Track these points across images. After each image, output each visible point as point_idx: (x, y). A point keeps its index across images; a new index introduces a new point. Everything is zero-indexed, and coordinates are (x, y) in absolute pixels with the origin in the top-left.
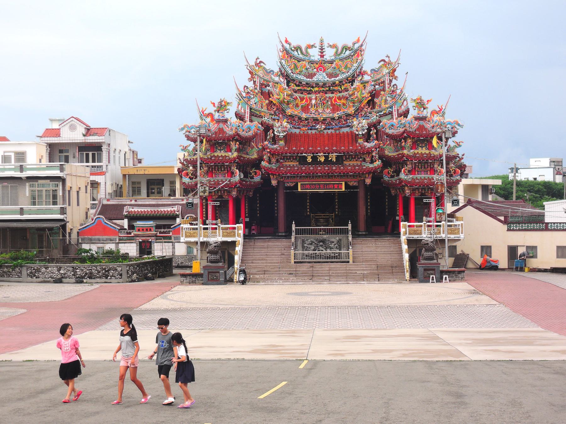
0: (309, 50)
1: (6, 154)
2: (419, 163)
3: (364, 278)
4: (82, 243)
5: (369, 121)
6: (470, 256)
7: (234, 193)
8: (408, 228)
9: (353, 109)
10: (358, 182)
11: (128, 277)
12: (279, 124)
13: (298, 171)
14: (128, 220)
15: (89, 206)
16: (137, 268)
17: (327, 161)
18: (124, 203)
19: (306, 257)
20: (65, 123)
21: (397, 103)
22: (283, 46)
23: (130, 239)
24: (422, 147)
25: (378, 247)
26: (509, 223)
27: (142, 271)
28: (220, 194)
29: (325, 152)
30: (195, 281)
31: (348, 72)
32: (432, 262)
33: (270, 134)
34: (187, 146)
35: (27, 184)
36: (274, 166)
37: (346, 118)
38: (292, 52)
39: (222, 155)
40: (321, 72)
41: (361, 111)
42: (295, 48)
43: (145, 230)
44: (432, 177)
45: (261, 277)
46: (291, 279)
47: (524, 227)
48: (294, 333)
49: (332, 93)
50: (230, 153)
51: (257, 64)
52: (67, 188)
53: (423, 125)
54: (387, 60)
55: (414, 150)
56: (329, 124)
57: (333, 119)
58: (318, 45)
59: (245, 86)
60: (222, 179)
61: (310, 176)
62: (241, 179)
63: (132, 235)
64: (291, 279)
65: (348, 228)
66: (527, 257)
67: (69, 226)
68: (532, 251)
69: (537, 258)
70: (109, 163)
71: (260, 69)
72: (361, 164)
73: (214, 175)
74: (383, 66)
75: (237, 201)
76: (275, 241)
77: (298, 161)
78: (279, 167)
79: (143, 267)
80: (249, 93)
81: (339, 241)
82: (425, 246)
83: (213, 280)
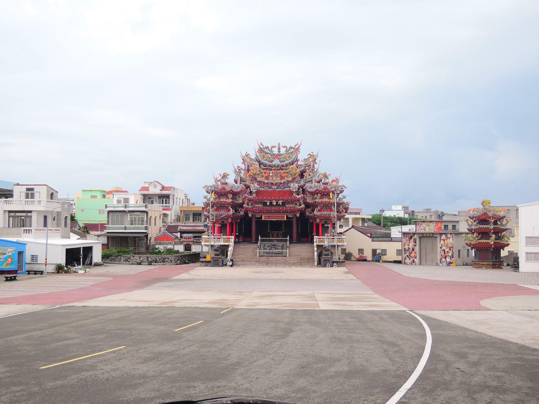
1: (119, 199)
3: (293, 264)
5: (300, 185)
6: (353, 254)
7: (229, 220)
8: (318, 239)
9: (291, 178)
12: (253, 185)
13: (262, 210)
15: (161, 226)
18: (179, 225)
20: (151, 184)
22: (259, 146)
23: (181, 243)
24: (326, 198)
26: (373, 238)
27: (183, 259)
29: (276, 200)
35: (129, 215)
36: (250, 207)
38: (264, 150)
41: (295, 179)
43: (188, 238)
48: (242, 292)
49: (282, 170)
50: (228, 200)
51: (246, 156)
52: (149, 217)
54: (312, 154)
56: (279, 186)
58: (277, 146)
59: (238, 166)
60: (223, 213)
62: (233, 213)
63: (181, 241)
65: (287, 239)
66: (381, 255)
67: (149, 236)
68: (384, 252)
70: (173, 204)
78: (253, 207)
79: (183, 257)
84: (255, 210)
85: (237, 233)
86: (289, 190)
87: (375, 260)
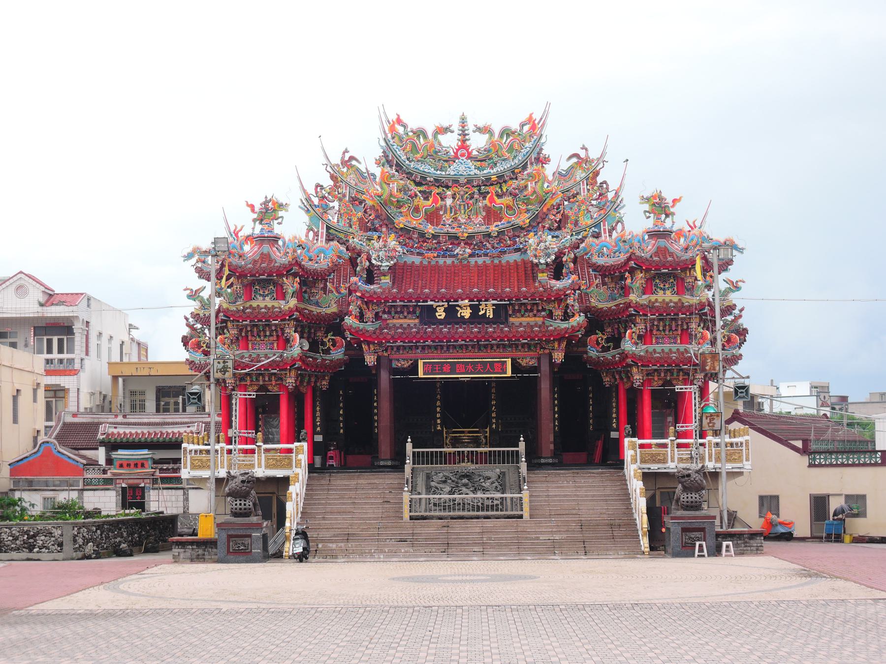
0: (440, 137)
2: (660, 320)
3: (552, 549)
4: (15, 490)
8: (638, 450)
9: (527, 215)
10: (539, 359)
11: (76, 550)
12: (381, 243)
13: (418, 336)
14: (106, 450)
16: (96, 531)
17: (476, 317)
19: (433, 508)
21: (608, 218)
25: (579, 487)
26: (811, 453)
27: (107, 537)
28: (261, 383)
30: (204, 555)
31: (515, 157)
32: (697, 513)
33: (361, 262)
34: (199, 289)
36: (370, 327)
37: (513, 234)
39: (266, 306)
40: (464, 158)
42: (414, 133)
43: (132, 466)
44: (685, 349)
45: (341, 547)
46: (403, 551)
47: (840, 460)
50: (282, 302)
51: (344, 163)
53: (666, 248)
54: (583, 154)
55: (648, 296)
56: (481, 246)
57: (488, 235)
58: (456, 127)
59: (318, 186)
61: (442, 346)
64: (403, 551)
65: (518, 452)
66: (847, 516)
69: (865, 516)
70: (87, 354)
71: (350, 171)
72: (543, 323)
73: (250, 346)
74: (576, 166)
75: (296, 397)
76: (371, 477)
77: (418, 317)
78: (381, 329)
79: (109, 530)
80: (326, 198)
81: (502, 476)
82: (683, 480)
83: (237, 552)
84: (389, 337)
85: (318, 433)
86: (519, 260)
87: (824, 535)
